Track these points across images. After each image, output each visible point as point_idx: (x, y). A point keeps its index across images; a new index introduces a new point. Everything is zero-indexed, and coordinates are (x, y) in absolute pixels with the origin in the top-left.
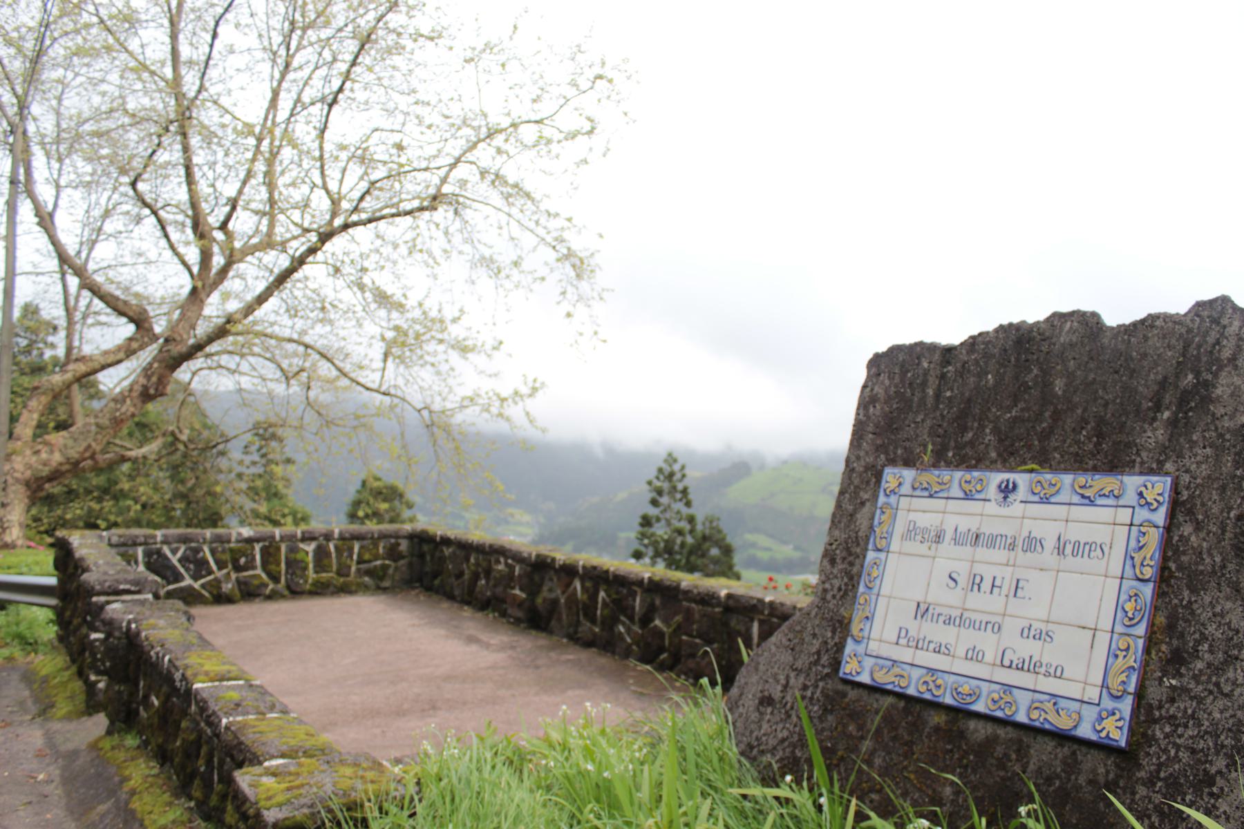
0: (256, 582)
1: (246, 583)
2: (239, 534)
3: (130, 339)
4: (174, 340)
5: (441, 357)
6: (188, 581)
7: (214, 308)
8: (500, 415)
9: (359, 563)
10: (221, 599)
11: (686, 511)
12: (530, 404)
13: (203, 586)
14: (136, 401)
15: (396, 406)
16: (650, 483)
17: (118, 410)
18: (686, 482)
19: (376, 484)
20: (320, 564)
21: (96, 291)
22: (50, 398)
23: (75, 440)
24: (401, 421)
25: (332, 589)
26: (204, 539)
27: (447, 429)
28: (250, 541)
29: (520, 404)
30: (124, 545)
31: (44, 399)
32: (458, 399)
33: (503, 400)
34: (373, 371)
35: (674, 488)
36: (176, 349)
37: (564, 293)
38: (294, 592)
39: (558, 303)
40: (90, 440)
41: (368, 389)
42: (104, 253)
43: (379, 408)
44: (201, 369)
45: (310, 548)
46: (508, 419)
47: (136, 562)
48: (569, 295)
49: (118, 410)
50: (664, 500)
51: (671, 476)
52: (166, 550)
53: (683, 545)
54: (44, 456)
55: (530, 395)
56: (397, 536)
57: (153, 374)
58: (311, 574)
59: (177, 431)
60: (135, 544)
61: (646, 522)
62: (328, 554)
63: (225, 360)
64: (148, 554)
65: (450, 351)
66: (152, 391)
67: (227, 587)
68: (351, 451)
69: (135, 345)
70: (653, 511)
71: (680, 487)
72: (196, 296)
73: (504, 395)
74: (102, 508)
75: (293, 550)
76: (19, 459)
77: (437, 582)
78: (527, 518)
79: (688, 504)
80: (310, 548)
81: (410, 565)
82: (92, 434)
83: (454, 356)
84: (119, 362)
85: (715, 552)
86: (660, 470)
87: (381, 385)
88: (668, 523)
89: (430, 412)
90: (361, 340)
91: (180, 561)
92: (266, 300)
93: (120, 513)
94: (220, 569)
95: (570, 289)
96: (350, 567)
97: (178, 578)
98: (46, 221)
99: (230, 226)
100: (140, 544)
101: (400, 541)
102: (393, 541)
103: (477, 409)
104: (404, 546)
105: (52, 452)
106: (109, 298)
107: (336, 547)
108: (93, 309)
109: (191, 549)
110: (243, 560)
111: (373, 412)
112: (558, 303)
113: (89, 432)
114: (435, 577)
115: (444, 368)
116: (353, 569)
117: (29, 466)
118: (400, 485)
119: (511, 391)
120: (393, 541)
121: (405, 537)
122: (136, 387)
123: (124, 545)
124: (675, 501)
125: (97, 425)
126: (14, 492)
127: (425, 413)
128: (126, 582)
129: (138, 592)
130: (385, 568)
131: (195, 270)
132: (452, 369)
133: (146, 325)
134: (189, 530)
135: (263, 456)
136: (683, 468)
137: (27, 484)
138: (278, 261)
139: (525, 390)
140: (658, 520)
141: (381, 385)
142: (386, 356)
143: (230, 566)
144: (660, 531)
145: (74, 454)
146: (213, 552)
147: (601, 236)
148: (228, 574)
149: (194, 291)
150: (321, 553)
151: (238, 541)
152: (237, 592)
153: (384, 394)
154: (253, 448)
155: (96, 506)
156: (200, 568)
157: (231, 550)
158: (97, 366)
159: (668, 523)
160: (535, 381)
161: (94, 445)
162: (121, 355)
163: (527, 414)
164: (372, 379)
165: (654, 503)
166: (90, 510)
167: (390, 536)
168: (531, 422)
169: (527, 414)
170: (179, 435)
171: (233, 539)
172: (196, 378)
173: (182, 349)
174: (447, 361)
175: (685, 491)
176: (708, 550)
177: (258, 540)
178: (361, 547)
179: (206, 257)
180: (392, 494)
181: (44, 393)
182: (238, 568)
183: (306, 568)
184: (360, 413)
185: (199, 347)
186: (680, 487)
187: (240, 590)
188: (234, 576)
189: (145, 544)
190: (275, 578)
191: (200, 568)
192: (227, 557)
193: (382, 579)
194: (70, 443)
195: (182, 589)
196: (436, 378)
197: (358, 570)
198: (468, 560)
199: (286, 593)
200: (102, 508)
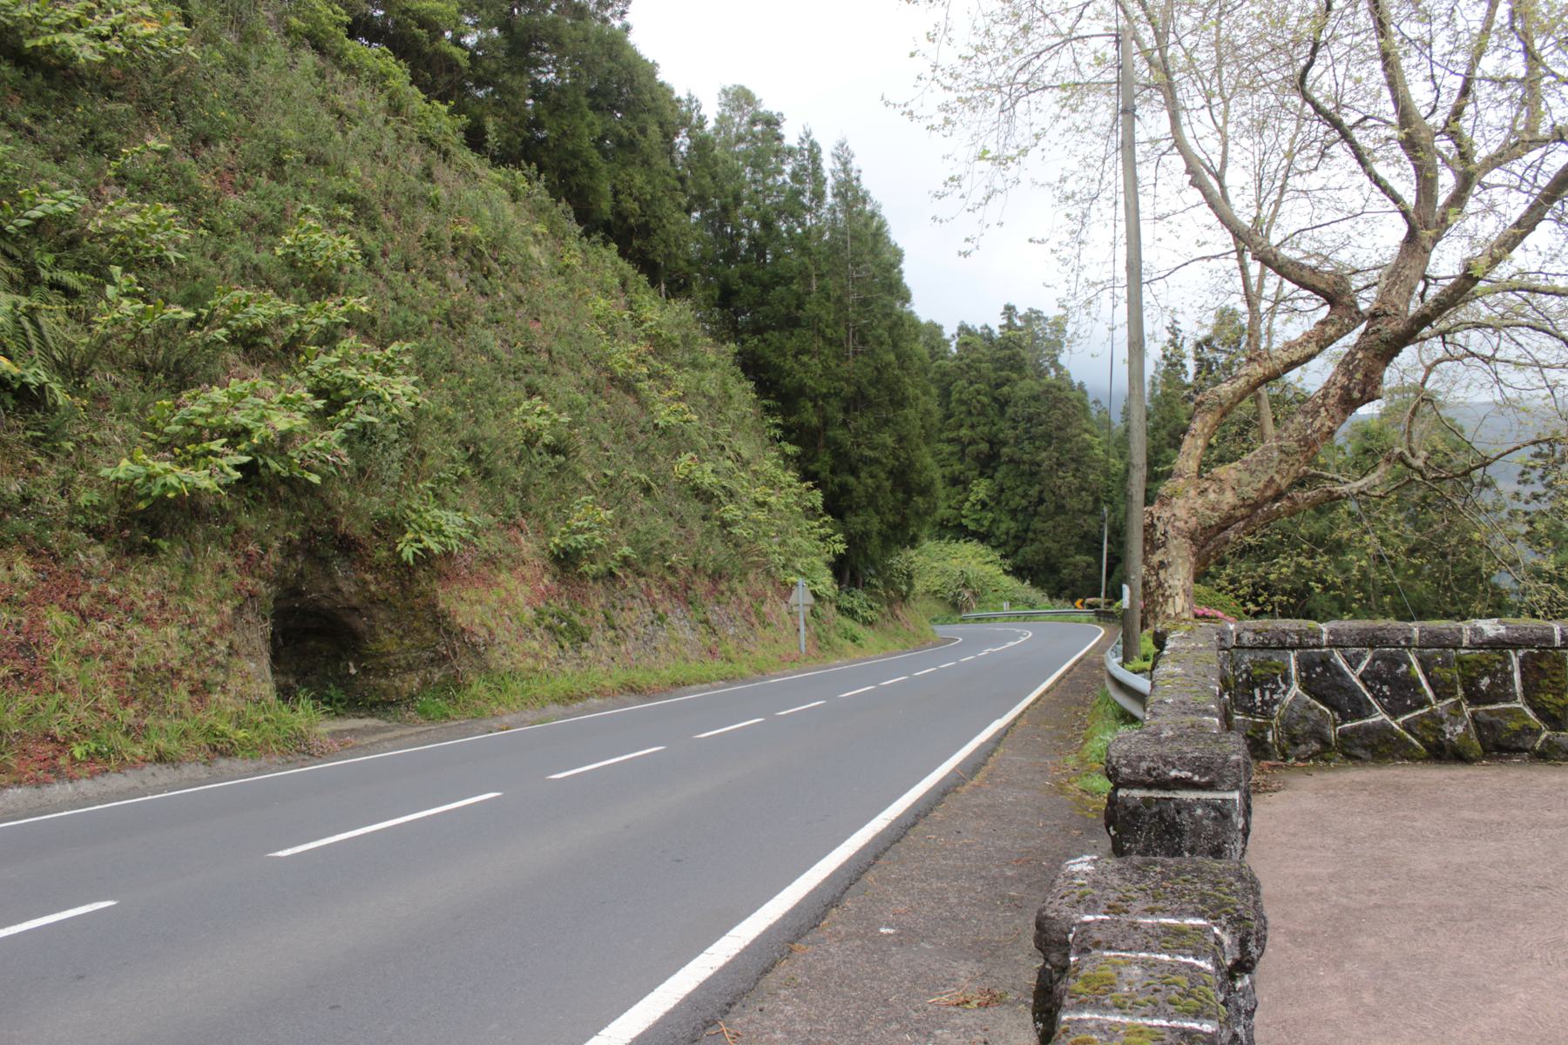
1: (1491, 726)
2: (1477, 631)
3: (1323, 323)
4: (1385, 314)
6: (1380, 716)
7: (1446, 260)
10: (1442, 753)
13: (1407, 726)
21: (1285, 270)
22: (1217, 416)
23: (1252, 473)
26: (1408, 639)
28: (1497, 644)
30: (1264, 647)
31: (1210, 419)
36: (1389, 328)
40: (1272, 472)
42: (1293, 216)
44: (1439, 361)
47: (1286, 679)
52: (1338, 658)
54: (1212, 496)
59: (1407, 453)
60: (1283, 647)
63: (1475, 340)
64: (1306, 665)
67: (1455, 731)
69: (1330, 330)
72: (1416, 244)
76: (1181, 502)
82: (1275, 464)
84: (1310, 357)
91: (1361, 678)
92: (1532, 228)
94: (1438, 696)
97: (1360, 709)
98: (1206, 181)
99: (1466, 125)
100: (1292, 648)
105: (1222, 491)
108: (1286, 292)
109: (1383, 657)
110: (1485, 682)
113: (1270, 459)
117: (1193, 512)
122: (1332, 391)
123: (1264, 647)
125: (1281, 450)
126: (1176, 547)
128: (1183, 762)
129: (1209, 786)
131: (1410, 198)
133: (1346, 299)
134: (1381, 622)
135: (1550, 486)
137: (1192, 537)
143: (1460, 692)
145: (1250, 492)
146: (1426, 665)
148: (1458, 705)
149: (1412, 238)
151: (1474, 646)
154: (1535, 475)
155: (1308, 563)
156: (1401, 693)
157: (1461, 662)
158: (1278, 366)
161: (1277, 478)
162: (1312, 347)
170: (1411, 460)
171: (1465, 642)
172: (1433, 376)
173: (1397, 326)
177: (1516, 646)
179: (1426, 185)
181: (1210, 410)
182: (1475, 697)
185: (1424, 320)
187: (1481, 738)
188: (1467, 711)
189: (1300, 646)
191: (1401, 693)
192: (1452, 674)
194: (1246, 477)
195: (1368, 730)
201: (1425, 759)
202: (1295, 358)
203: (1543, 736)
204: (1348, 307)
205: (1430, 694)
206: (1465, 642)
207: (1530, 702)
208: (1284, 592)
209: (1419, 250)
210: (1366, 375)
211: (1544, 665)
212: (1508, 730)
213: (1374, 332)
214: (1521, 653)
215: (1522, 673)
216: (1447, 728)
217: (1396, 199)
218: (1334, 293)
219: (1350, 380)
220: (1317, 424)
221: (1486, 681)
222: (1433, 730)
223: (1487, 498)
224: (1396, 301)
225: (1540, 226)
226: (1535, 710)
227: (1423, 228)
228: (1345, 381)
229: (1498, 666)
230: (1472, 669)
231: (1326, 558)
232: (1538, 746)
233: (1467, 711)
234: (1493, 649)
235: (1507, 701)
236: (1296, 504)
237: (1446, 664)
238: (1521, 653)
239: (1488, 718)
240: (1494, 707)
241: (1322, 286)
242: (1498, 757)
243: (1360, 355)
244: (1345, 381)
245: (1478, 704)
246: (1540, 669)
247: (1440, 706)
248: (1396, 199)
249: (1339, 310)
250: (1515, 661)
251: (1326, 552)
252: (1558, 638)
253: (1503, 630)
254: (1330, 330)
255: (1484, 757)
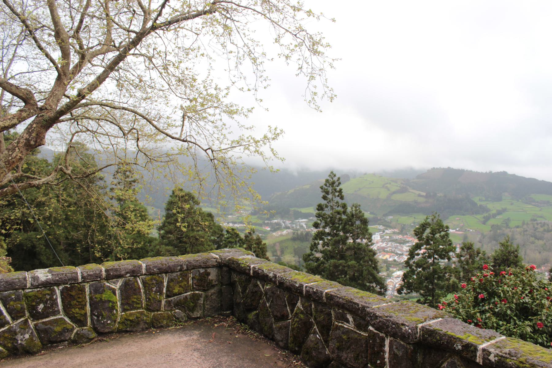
0: (58, 329)
1: (46, 331)
2: (35, 278)
4: (46, 109)
5: (218, 117)
8: (257, 151)
9: (168, 296)
11: (340, 202)
12: (274, 144)
14: (22, 149)
15: (191, 148)
16: (322, 188)
17: (10, 155)
18: (341, 187)
19: (181, 194)
20: (127, 304)
24: (194, 157)
25: (142, 325)
27: (224, 162)
28: (48, 285)
29: (268, 144)
32: (230, 142)
33: (256, 142)
34: (176, 127)
35: (335, 190)
37: (300, 68)
38: (103, 334)
39: (297, 75)
41: (173, 138)
43: (181, 150)
45: (117, 285)
46: (261, 154)
48: (304, 70)
49: (10, 155)
50: (330, 196)
51: (333, 183)
53: (340, 219)
55: (274, 139)
56: (206, 266)
57: (33, 131)
58: (119, 313)
61: (320, 208)
62: (136, 291)
63: (92, 125)
65: (222, 114)
66: (32, 143)
67: (23, 338)
68: (165, 176)
69: (24, 114)
70: (324, 202)
71: (338, 189)
73: (258, 138)
74: (30, 212)
75: (97, 290)
77: (251, 316)
78: (247, 203)
79: (342, 198)
80: (117, 285)
81: (220, 292)
83: (225, 117)
85: (358, 223)
86: (327, 181)
87: (181, 136)
88: (332, 208)
89: (212, 151)
90: (168, 107)
93: (40, 214)
94: (13, 319)
95: (305, 65)
96: (160, 301)
101: (209, 270)
102: (202, 271)
103: (242, 148)
104: (213, 274)
106: (14, 89)
107: (144, 283)
111: (177, 152)
112: (297, 75)
114: (250, 310)
115: (219, 124)
116: (163, 302)
118: (196, 194)
119: (262, 136)
120: (202, 271)
121: (213, 266)
122: (22, 140)
124: (335, 196)
127: (209, 152)
130: (195, 298)
132: (224, 125)
133: (32, 102)
136: (339, 178)
138: (111, 56)
139: (270, 135)
140: (327, 207)
141: (181, 136)
142: (183, 117)
143: (27, 314)
144: (328, 212)
147: (334, 20)
148: (26, 321)
149: (59, 79)
150: (128, 291)
151: (33, 287)
152: (37, 341)
153: (183, 141)
157: (27, 297)
159: (332, 208)
160: (276, 129)
162: (15, 121)
163: (272, 150)
164: (175, 131)
165: (324, 198)
166: (23, 214)
167: (200, 267)
168: (274, 154)
169: (272, 150)
170: (65, 171)
171: (28, 285)
173: (51, 114)
174: (221, 120)
175: (340, 191)
176: (355, 223)
177: (58, 285)
178: (170, 281)
180: (189, 198)
182: (35, 316)
183: (113, 308)
184: (170, 153)
185: (62, 112)
186: (338, 189)
188: (31, 324)
190: (81, 322)
193: (192, 310)
196: (215, 129)
197: (168, 303)
198: (293, 305)
199: (94, 335)
200: (30, 212)
201: (7, 357)
202: (6, 125)
203: (75, 331)
204: (33, 105)
205: (8, 318)
206: (28, 285)
207: (67, 313)
208: (18, 224)
209: (62, 84)
210: (37, 135)
211: (73, 293)
212: (55, 332)
213: (41, 116)
214: (61, 288)
215: (62, 298)
216: (19, 337)
217: (54, 63)
218: (27, 98)
219: (30, 136)
220: (14, 155)
221: (41, 306)
222: (11, 339)
223: (101, 183)
224: (51, 104)
225: (107, 79)
226: (70, 318)
227: (64, 76)
228: (27, 136)
229: (48, 297)
230: (33, 301)
231: (35, 209)
232: (72, 336)
233: (31, 324)
234: (45, 287)
235: (55, 315)
236: (14, 188)
237: (18, 299)
238: (61, 288)
239: (44, 327)
240: (47, 320)
241: (21, 95)
242: (52, 347)
243: (34, 126)
244: (27, 136)
245: (38, 319)
246: (71, 295)
247: (14, 324)
248: (54, 63)
249: (28, 106)
250: (58, 292)
251: (35, 207)
252: (80, 277)
253: (50, 276)
254: (24, 114)
255: (43, 349)
